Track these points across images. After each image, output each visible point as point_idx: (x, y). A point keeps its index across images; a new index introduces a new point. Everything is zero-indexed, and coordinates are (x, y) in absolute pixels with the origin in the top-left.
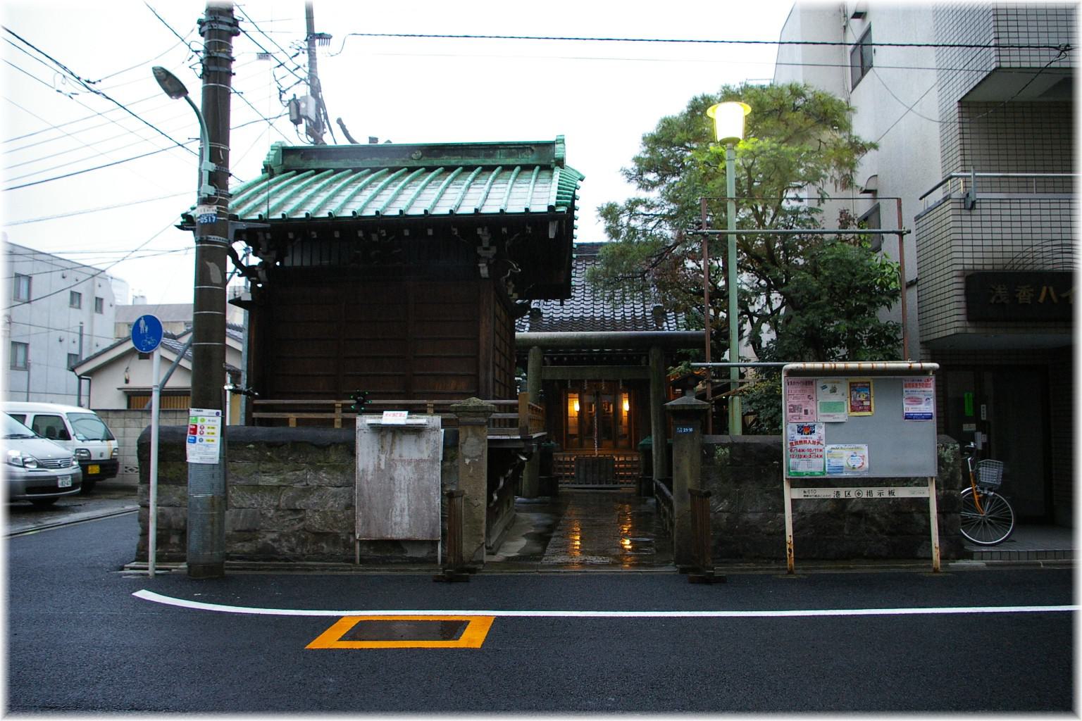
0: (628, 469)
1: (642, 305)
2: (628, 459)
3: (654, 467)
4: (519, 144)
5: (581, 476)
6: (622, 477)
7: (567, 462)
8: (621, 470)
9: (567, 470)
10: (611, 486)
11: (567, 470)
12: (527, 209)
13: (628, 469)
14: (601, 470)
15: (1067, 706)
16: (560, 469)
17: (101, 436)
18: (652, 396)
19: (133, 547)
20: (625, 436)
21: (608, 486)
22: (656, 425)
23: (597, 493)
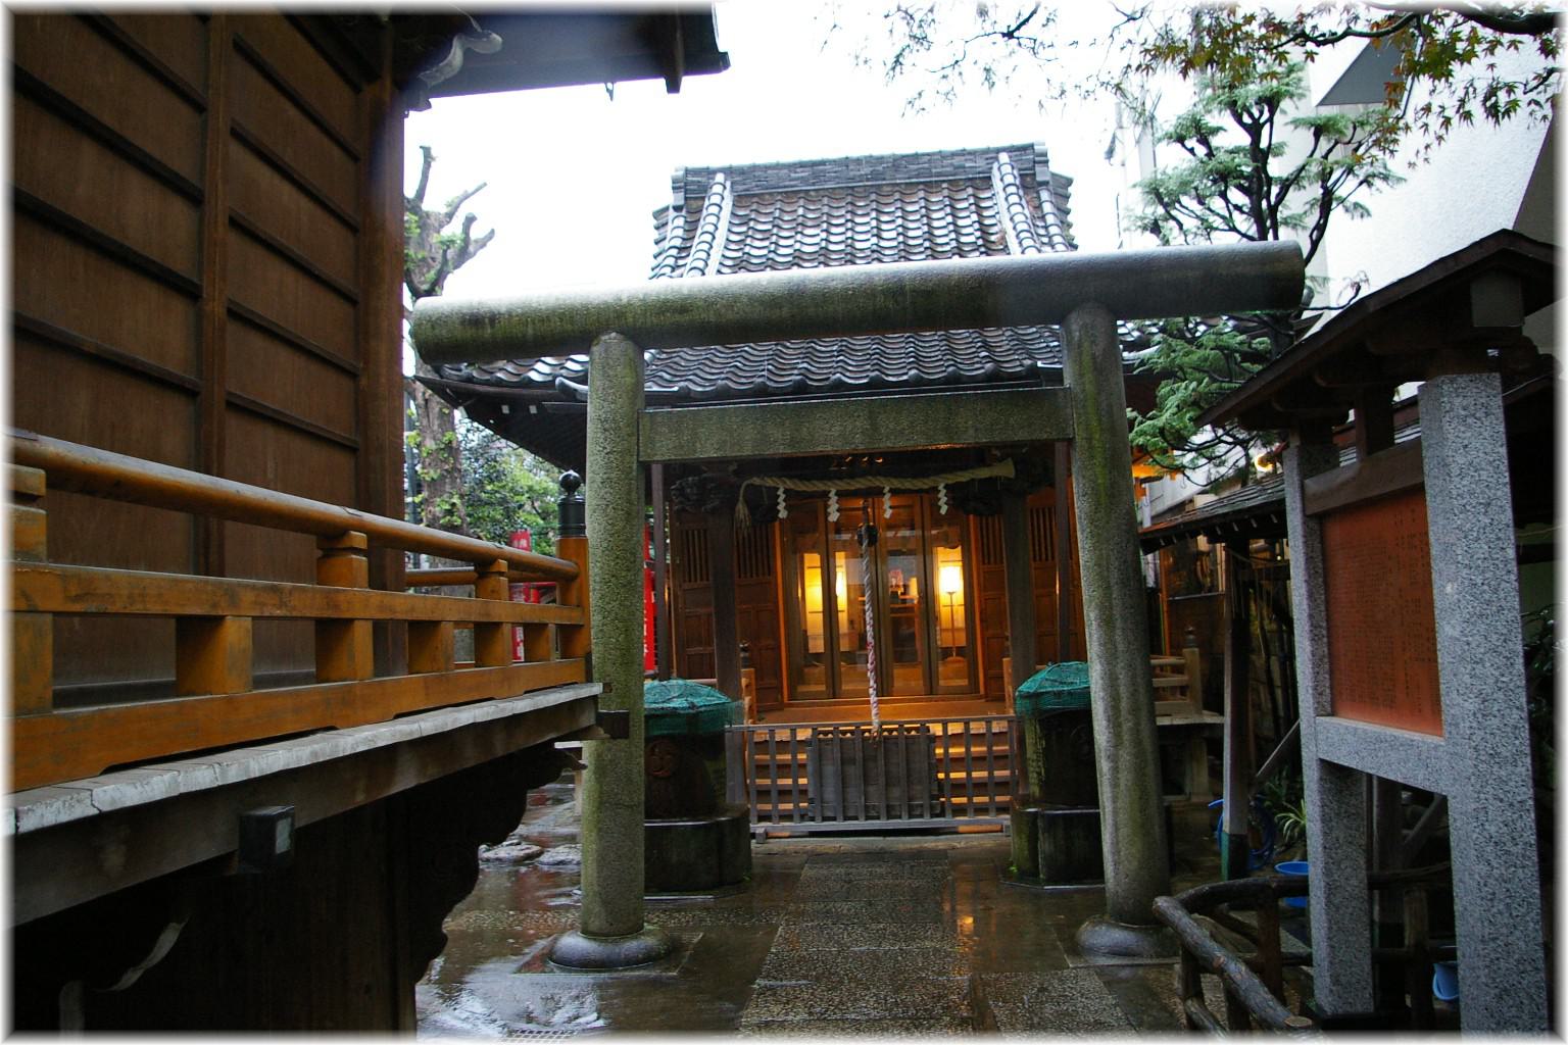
0: (979, 760)
1: (950, 219)
2: (977, 728)
3: (1104, 766)
4: (898, 162)
5: (830, 794)
6: (959, 788)
7: (783, 746)
8: (957, 763)
9: (784, 769)
10: (926, 822)
11: (784, 769)
12: (673, 86)
13: (979, 760)
14: (892, 771)
15: (22, 22)
16: (762, 769)
17: (356, 622)
18: (1081, 506)
19: (344, 750)
20: (960, 651)
21: (916, 823)
22: (1107, 622)
23: (878, 856)
